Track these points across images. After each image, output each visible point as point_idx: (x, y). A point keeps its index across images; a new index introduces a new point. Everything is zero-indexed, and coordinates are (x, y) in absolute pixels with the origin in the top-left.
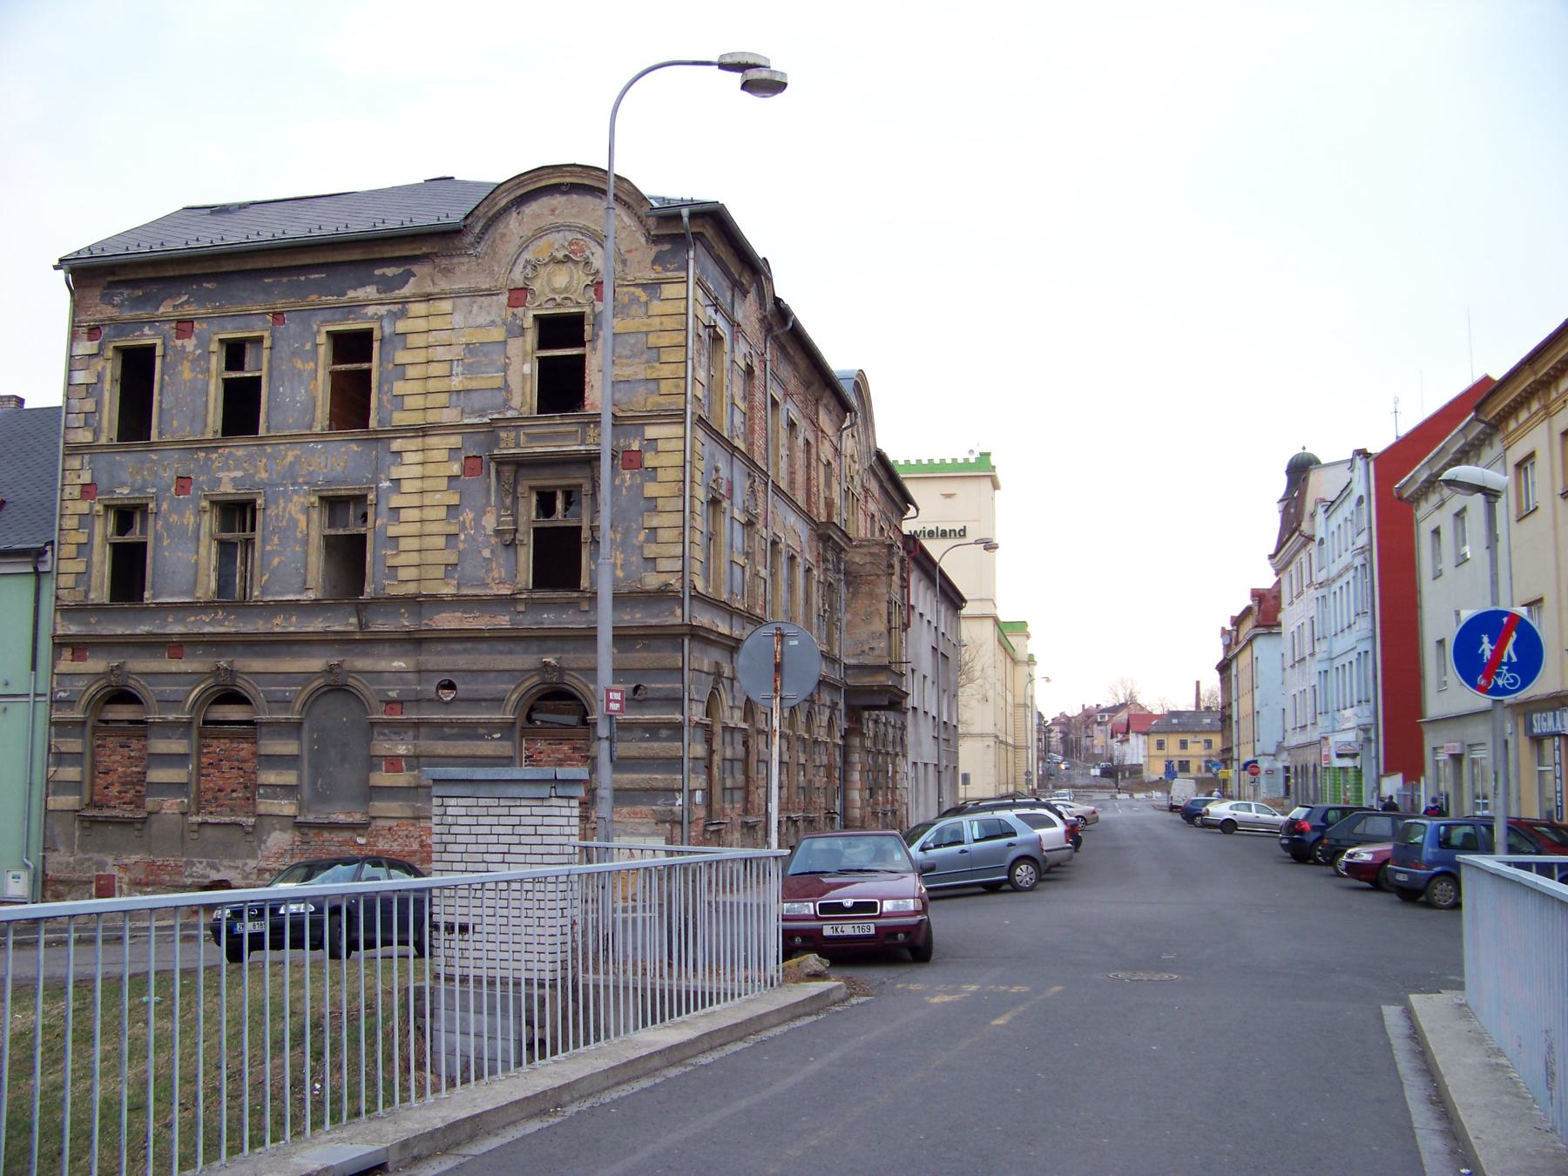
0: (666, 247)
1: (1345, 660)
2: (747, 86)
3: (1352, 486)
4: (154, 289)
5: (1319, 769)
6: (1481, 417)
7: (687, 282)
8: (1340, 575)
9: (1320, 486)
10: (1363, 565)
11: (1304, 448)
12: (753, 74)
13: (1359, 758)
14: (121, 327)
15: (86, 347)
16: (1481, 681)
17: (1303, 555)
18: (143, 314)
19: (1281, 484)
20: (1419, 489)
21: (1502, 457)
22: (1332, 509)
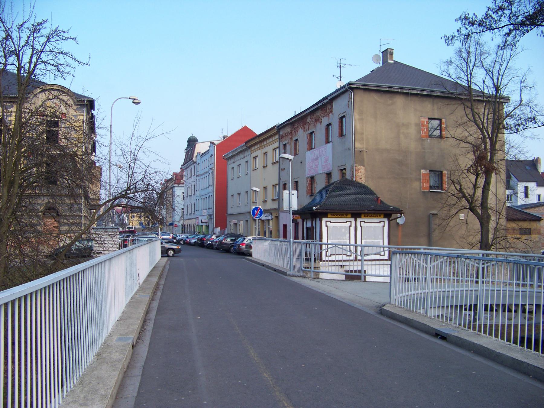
0: (79, 107)
1: (205, 197)
2: (134, 103)
3: (209, 151)
5: (195, 225)
6: (246, 145)
7: (84, 115)
8: (204, 174)
9: (200, 148)
10: (212, 173)
11: (193, 135)
12: (135, 101)
13: (208, 223)
16: (255, 216)
17: (193, 166)
19: (186, 145)
20: (229, 157)
21: (250, 155)
22: (202, 156)
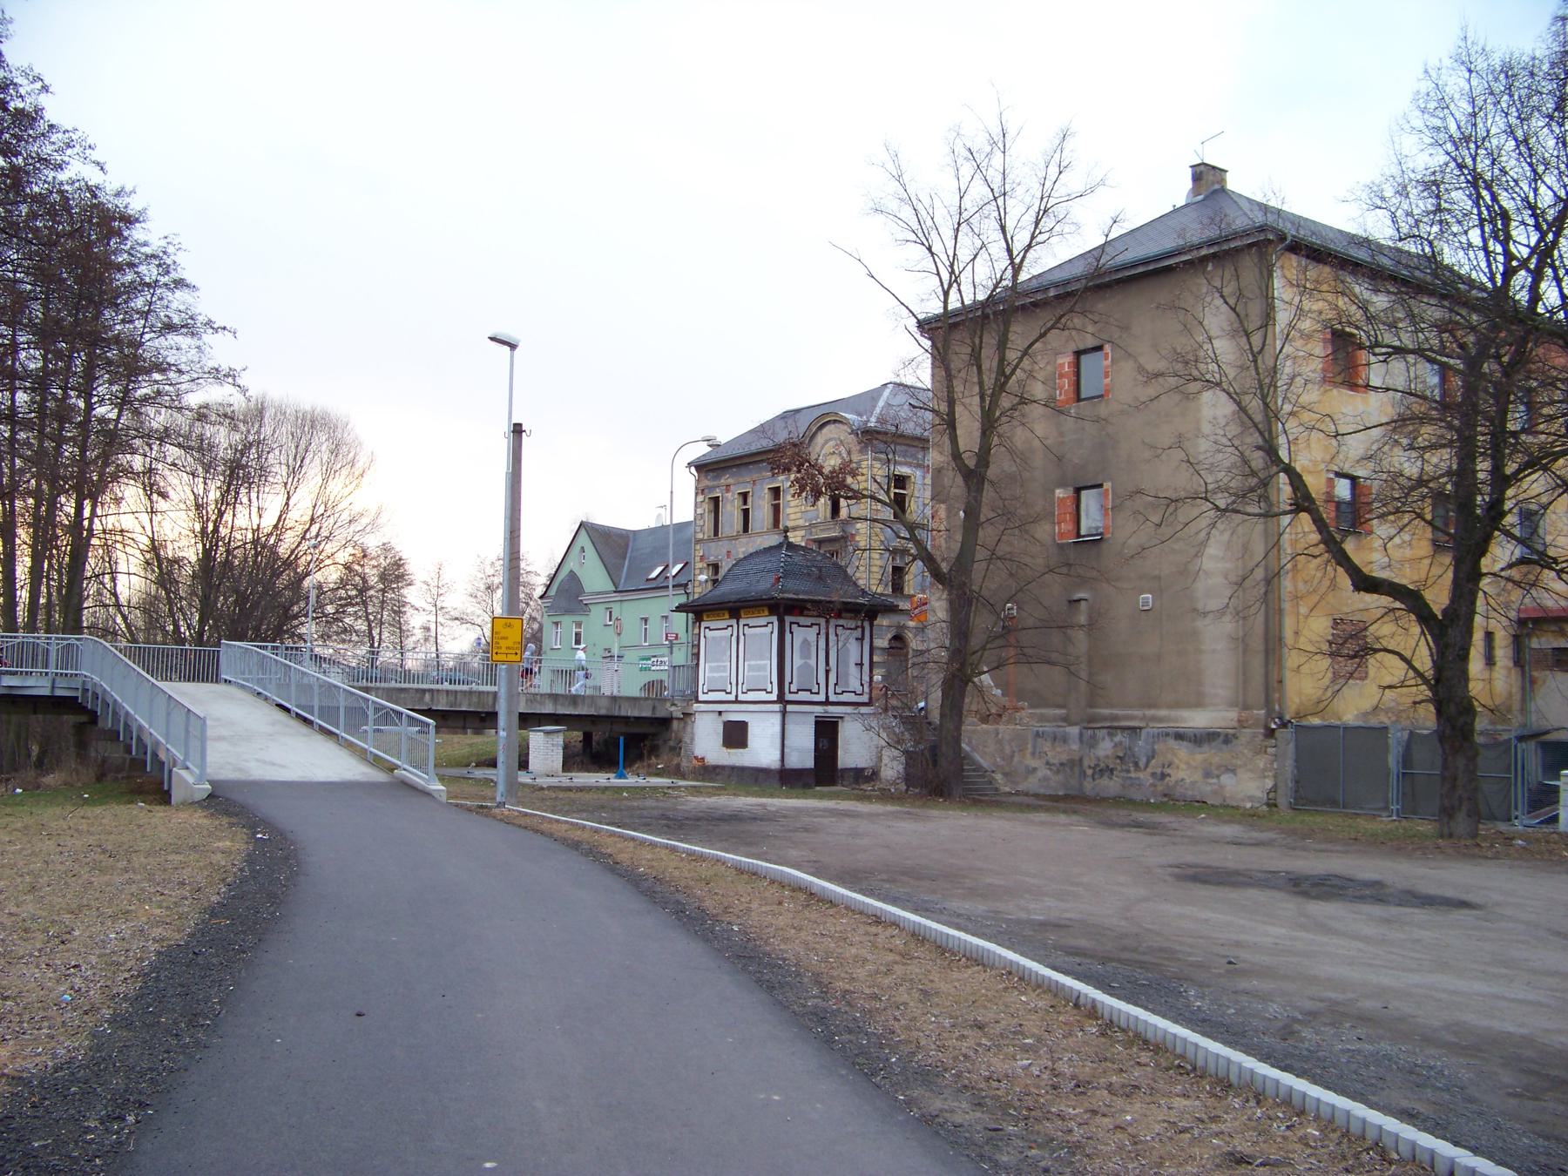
4: (719, 472)
14: (712, 489)
15: (700, 498)
18: (715, 483)
